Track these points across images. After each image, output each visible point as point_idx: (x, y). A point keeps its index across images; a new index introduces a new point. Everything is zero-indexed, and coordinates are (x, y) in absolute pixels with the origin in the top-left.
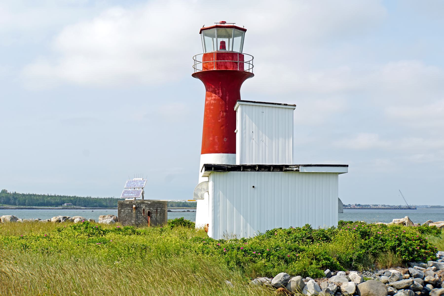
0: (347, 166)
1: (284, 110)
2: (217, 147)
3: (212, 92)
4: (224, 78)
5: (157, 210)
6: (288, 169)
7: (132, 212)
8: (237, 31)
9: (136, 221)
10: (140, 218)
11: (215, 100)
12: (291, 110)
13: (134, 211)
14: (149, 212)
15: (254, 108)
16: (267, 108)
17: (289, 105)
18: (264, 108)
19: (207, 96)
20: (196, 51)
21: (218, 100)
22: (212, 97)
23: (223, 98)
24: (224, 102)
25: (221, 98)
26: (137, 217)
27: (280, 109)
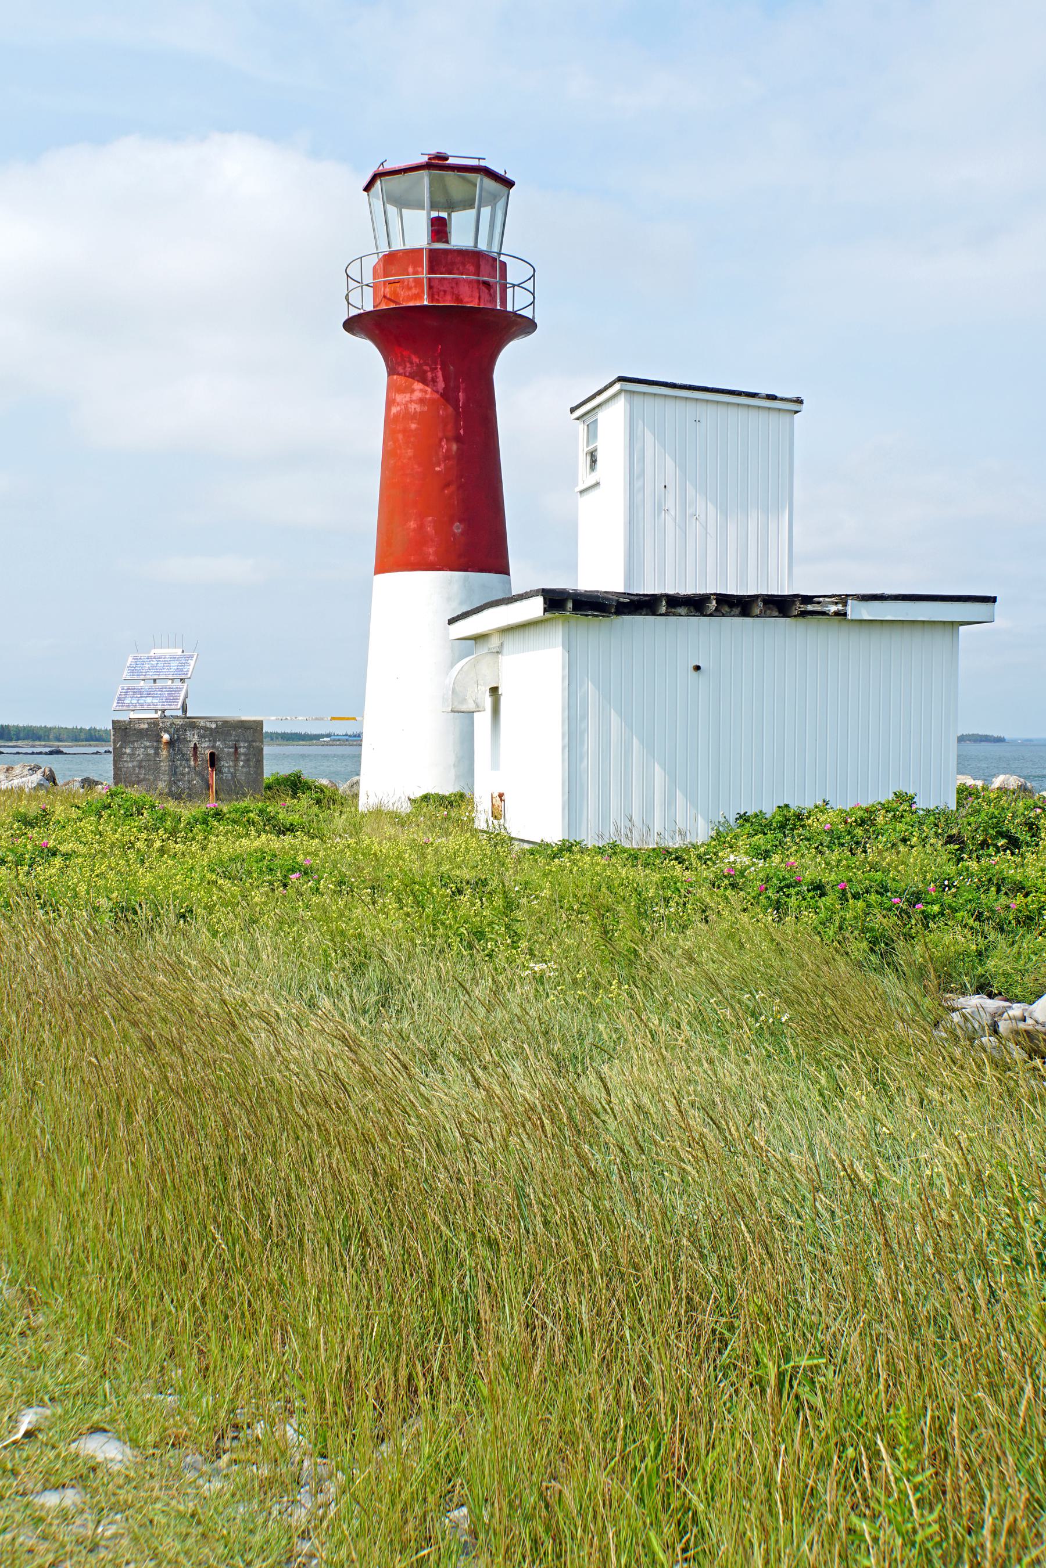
0: (993, 600)
1: (763, 415)
2: (431, 550)
3: (412, 376)
4: (444, 331)
5: (236, 749)
6: (810, 608)
7: (157, 754)
8: (489, 184)
9: (170, 784)
10: (183, 775)
11: (421, 401)
12: (788, 416)
13: (164, 753)
14: (212, 755)
15: (670, 404)
16: (711, 409)
17: (782, 399)
18: (701, 408)
19: (391, 388)
20: (356, 240)
21: (432, 401)
22: (412, 391)
23: (448, 396)
24: (450, 410)
25: (442, 395)
26: (174, 770)
27: (753, 414)
